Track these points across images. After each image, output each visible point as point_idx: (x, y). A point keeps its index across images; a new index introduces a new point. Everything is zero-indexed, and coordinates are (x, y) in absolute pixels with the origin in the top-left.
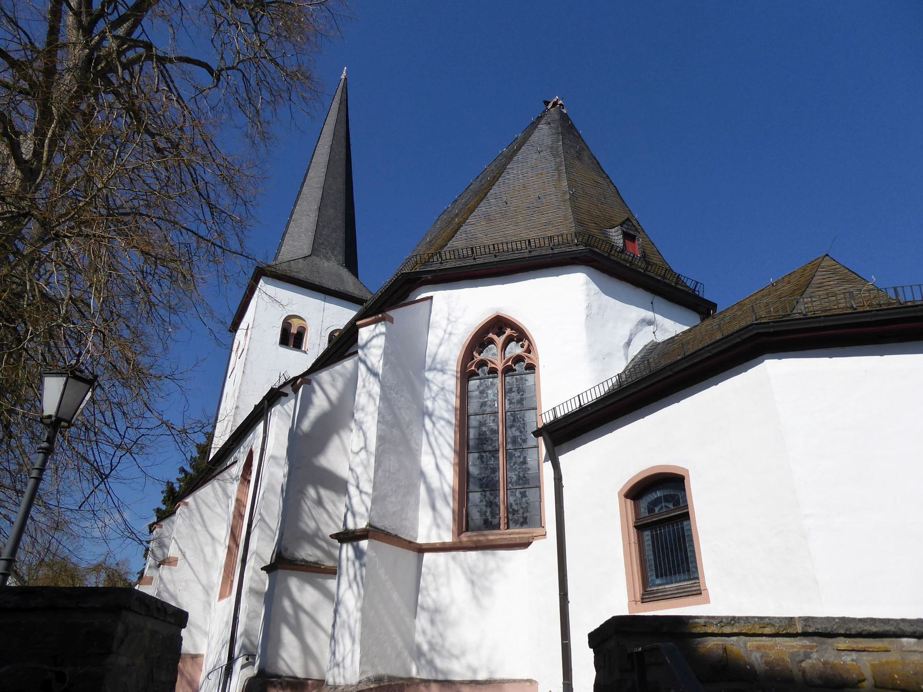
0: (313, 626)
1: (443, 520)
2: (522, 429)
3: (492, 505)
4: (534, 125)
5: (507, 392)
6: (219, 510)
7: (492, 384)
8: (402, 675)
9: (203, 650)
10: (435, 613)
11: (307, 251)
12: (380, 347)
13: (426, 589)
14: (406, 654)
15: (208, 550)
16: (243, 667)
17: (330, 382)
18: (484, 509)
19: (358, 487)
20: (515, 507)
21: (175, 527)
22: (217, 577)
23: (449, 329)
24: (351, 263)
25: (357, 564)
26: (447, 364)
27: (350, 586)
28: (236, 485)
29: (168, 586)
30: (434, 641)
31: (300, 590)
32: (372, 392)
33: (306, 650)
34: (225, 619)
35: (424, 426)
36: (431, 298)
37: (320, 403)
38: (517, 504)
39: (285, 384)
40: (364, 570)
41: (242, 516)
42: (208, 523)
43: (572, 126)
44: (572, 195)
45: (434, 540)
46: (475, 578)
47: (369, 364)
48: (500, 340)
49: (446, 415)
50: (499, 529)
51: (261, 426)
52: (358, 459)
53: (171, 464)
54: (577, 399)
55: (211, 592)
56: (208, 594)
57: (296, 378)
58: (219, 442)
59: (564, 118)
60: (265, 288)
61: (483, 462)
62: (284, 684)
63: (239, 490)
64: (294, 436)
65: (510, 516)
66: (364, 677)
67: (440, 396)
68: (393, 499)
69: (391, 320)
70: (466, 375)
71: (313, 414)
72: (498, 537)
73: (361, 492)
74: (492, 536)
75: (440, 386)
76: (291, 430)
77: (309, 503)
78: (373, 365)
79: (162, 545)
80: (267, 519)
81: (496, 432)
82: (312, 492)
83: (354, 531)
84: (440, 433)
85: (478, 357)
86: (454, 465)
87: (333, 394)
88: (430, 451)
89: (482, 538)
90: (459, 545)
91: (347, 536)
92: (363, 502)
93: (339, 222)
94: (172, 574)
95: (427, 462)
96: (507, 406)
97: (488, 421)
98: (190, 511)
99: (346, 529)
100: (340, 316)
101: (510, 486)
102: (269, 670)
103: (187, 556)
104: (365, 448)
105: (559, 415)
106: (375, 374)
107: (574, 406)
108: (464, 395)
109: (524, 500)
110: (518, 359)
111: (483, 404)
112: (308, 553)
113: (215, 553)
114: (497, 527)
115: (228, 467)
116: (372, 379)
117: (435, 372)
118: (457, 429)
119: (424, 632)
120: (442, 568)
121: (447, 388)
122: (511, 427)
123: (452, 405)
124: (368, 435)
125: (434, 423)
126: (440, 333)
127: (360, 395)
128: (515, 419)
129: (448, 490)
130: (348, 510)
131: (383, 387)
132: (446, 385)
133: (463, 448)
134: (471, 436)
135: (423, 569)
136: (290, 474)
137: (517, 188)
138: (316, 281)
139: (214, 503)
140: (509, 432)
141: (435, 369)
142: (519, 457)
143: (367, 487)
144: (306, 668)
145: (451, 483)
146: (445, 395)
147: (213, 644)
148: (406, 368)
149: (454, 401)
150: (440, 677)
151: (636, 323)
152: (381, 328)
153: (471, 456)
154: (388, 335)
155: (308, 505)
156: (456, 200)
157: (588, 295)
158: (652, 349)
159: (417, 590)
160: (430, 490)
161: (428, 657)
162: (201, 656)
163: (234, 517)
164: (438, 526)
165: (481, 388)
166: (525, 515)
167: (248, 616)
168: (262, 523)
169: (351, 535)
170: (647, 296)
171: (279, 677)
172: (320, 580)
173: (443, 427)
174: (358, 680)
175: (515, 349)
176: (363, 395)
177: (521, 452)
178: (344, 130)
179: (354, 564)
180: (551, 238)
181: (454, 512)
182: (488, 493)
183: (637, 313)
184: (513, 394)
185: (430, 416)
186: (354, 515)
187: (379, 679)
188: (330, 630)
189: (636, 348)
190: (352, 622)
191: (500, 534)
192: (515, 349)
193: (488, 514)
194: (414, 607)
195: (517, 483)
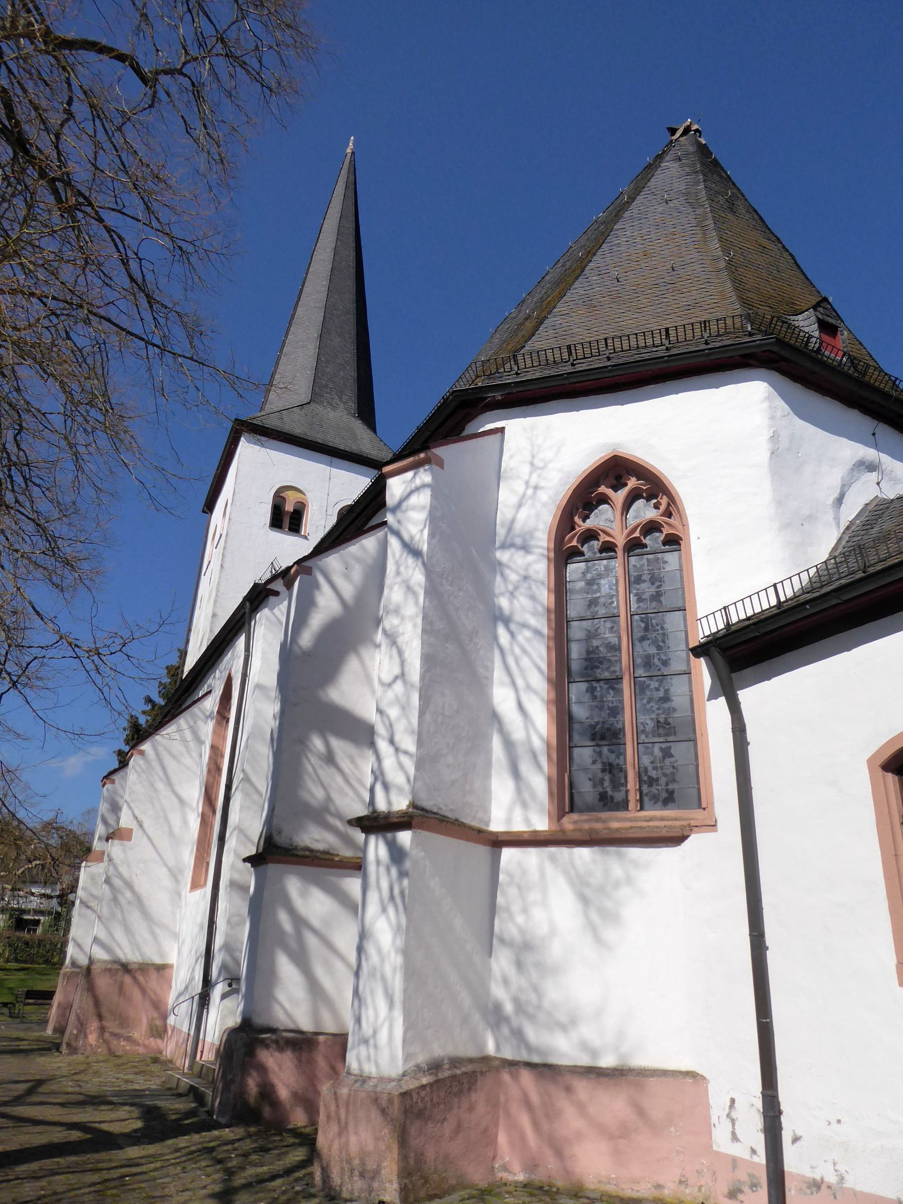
0: (324, 951)
1: (533, 796)
2: (661, 644)
3: (614, 770)
4: (650, 168)
5: (633, 581)
6: (188, 761)
7: (607, 569)
8: (470, 1052)
9: (173, 959)
10: (525, 950)
11: (305, 397)
12: (423, 508)
13: (507, 909)
14: (476, 1017)
15: (175, 820)
16: (224, 996)
17: (344, 568)
18: (600, 775)
19: (392, 741)
20: (653, 774)
21: (129, 783)
22: (188, 857)
23: (534, 480)
24: (366, 412)
25: (394, 871)
26: (532, 537)
27: (384, 910)
28: (211, 724)
29: (121, 869)
30: (523, 997)
31: (304, 894)
32: (412, 582)
33: (314, 988)
34: (199, 920)
35: (496, 638)
36: (502, 430)
37: (327, 604)
38: (655, 768)
39: (274, 578)
40: (406, 882)
41: (219, 770)
42: (174, 779)
43: (716, 163)
44: (729, 262)
45: (519, 826)
46: (588, 892)
47: (406, 537)
48: (619, 497)
49: (532, 621)
50: (626, 808)
51: (241, 641)
52: (390, 694)
53: (140, 693)
54: (771, 591)
55: (180, 878)
56: (177, 881)
57: (289, 569)
58: (191, 662)
59: (704, 151)
60: (249, 454)
61: (594, 698)
62: (282, 1042)
63: (214, 732)
64: (289, 655)
65: (645, 788)
66: (411, 1064)
67: (522, 590)
68: (450, 759)
69: (440, 463)
70: (563, 555)
71: (317, 621)
72: (628, 824)
73: (397, 750)
74: (617, 822)
75: (522, 572)
76: (283, 646)
77: (313, 759)
78: (412, 538)
79: (115, 808)
80: (254, 778)
81: (617, 648)
82: (317, 743)
83: (388, 815)
84: (524, 651)
85: (582, 526)
86: (549, 702)
87: (348, 590)
88: (506, 679)
89: (598, 826)
90: (560, 837)
91: (376, 823)
92: (401, 766)
93: (350, 296)
94: (124, 852)
95: (502, 698)
96: (634, 606)
97: (602, 630)
98: (147, 761)
99: (375, 811)
100: (352, 485)
101: (643, 738)
102: (260, 1020)
103: (146, 826)
104: (402, 676)
105: (734, 619)
106: (415, 552)
107: (768, 602)
108: (560, 588)
109: (668, 761)
110: (651, 527)
111: (593, 603)
112: (314, 837)
113: (185, 822)
114: (624, 805)
115: (199, 699)
116: (410, 561)
117: (513, 550)
118: (552, 644)
119: (506, 982)
120: (534, 876)
121: (534, 576)
122: (643, 639)
123: (543, 605)
124: (407, 654)
125: (512, 635)
126: (520, 487)
127: (391, 589)
128: (649, 629)
129: (538, 744)
130: (376, 779)
131: (429, 573)
132: (531, 572)
133: (561, 675)
134: (574, 655)
135: (502, 877)
136: (283, 714)
137: (633, 257)
138: (319, 438)
139: (182, 751)
140: (638, 648)
141: (512, 545)
142: (657, 689)
143: (409, 743)
144: (316, 1017)
145: (544, 731)
146: (530, 588)
147: (186, 949)
148: (466, 546)
149: (545, 597)
150: (536, 1059)
151: (850, 465)
152: (424, 476)
153: (574, 687)
154: (435, 488)
155: (312, 763)
156: (523, 301)
157: (772, 418)
158: (878, 511)
159: (492, 909)
160: (509, 745)
161: (515, 1022)
162: (170, 966)
163: (209, 771)
164: (525, 805)
165: (589, 576)
166: (671, 787)
167: (229, 922)
168: (247, 785)
169: (382, 822)
170: (866, 423)
171: (273, 1030)
172: (333, 879)
173: (528, 640)
174: (400, 1071)
175: (643, 511)
176: (396, 587)
177: (661, 682)
178: (352, 225)
179: (388, 870)
180: (705, 324)
181: (549, 780)
182: (605, 750)
183: (850, 450)
184: (644, 586)
185: (507, 621)
186: (386, 787)
187: (435, 1066)
188: (352, 957)
189: (852, 510)
190: (388, 970)
191: (630, 820)
192: (643, 511)
193: (607, 783)
194: (489, 939)
195: (655, 733)
